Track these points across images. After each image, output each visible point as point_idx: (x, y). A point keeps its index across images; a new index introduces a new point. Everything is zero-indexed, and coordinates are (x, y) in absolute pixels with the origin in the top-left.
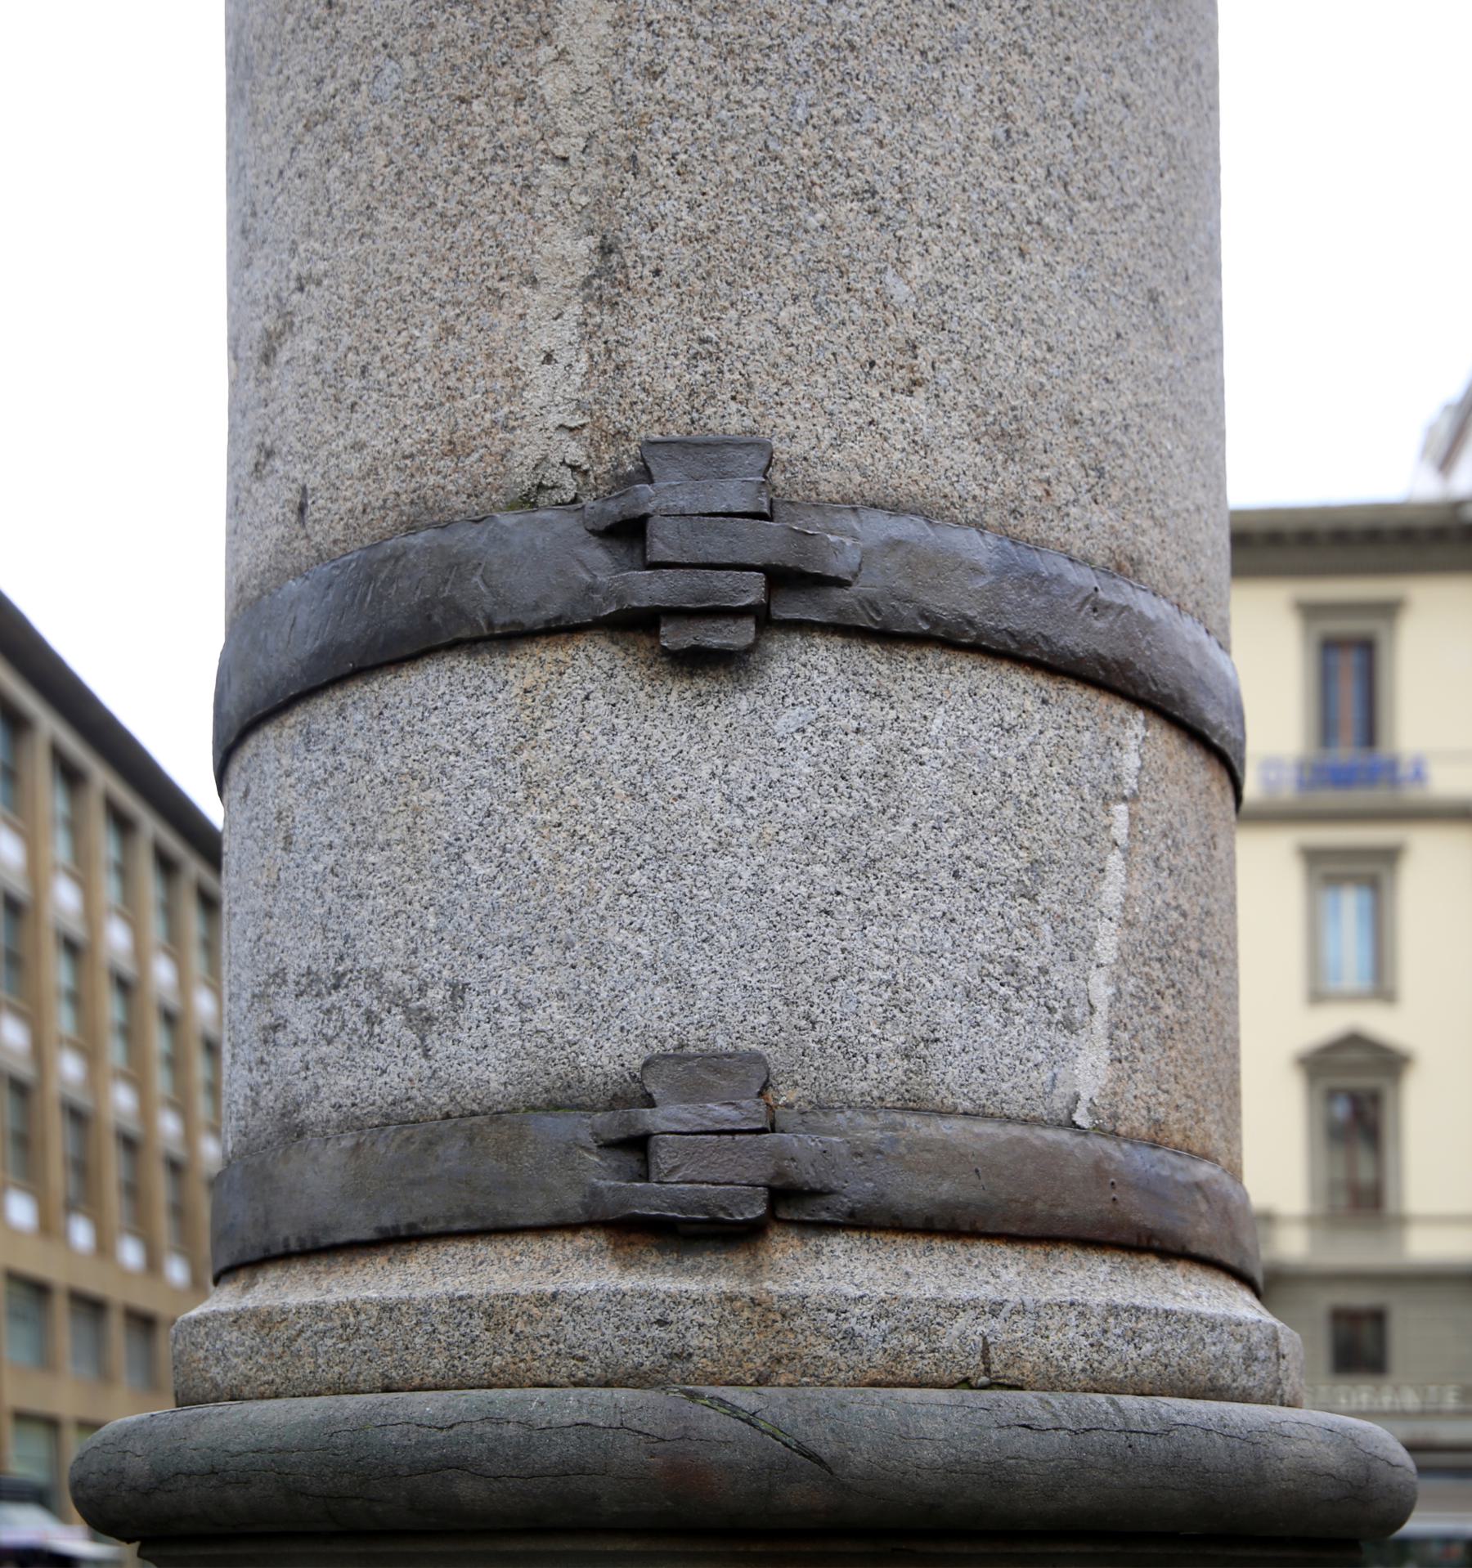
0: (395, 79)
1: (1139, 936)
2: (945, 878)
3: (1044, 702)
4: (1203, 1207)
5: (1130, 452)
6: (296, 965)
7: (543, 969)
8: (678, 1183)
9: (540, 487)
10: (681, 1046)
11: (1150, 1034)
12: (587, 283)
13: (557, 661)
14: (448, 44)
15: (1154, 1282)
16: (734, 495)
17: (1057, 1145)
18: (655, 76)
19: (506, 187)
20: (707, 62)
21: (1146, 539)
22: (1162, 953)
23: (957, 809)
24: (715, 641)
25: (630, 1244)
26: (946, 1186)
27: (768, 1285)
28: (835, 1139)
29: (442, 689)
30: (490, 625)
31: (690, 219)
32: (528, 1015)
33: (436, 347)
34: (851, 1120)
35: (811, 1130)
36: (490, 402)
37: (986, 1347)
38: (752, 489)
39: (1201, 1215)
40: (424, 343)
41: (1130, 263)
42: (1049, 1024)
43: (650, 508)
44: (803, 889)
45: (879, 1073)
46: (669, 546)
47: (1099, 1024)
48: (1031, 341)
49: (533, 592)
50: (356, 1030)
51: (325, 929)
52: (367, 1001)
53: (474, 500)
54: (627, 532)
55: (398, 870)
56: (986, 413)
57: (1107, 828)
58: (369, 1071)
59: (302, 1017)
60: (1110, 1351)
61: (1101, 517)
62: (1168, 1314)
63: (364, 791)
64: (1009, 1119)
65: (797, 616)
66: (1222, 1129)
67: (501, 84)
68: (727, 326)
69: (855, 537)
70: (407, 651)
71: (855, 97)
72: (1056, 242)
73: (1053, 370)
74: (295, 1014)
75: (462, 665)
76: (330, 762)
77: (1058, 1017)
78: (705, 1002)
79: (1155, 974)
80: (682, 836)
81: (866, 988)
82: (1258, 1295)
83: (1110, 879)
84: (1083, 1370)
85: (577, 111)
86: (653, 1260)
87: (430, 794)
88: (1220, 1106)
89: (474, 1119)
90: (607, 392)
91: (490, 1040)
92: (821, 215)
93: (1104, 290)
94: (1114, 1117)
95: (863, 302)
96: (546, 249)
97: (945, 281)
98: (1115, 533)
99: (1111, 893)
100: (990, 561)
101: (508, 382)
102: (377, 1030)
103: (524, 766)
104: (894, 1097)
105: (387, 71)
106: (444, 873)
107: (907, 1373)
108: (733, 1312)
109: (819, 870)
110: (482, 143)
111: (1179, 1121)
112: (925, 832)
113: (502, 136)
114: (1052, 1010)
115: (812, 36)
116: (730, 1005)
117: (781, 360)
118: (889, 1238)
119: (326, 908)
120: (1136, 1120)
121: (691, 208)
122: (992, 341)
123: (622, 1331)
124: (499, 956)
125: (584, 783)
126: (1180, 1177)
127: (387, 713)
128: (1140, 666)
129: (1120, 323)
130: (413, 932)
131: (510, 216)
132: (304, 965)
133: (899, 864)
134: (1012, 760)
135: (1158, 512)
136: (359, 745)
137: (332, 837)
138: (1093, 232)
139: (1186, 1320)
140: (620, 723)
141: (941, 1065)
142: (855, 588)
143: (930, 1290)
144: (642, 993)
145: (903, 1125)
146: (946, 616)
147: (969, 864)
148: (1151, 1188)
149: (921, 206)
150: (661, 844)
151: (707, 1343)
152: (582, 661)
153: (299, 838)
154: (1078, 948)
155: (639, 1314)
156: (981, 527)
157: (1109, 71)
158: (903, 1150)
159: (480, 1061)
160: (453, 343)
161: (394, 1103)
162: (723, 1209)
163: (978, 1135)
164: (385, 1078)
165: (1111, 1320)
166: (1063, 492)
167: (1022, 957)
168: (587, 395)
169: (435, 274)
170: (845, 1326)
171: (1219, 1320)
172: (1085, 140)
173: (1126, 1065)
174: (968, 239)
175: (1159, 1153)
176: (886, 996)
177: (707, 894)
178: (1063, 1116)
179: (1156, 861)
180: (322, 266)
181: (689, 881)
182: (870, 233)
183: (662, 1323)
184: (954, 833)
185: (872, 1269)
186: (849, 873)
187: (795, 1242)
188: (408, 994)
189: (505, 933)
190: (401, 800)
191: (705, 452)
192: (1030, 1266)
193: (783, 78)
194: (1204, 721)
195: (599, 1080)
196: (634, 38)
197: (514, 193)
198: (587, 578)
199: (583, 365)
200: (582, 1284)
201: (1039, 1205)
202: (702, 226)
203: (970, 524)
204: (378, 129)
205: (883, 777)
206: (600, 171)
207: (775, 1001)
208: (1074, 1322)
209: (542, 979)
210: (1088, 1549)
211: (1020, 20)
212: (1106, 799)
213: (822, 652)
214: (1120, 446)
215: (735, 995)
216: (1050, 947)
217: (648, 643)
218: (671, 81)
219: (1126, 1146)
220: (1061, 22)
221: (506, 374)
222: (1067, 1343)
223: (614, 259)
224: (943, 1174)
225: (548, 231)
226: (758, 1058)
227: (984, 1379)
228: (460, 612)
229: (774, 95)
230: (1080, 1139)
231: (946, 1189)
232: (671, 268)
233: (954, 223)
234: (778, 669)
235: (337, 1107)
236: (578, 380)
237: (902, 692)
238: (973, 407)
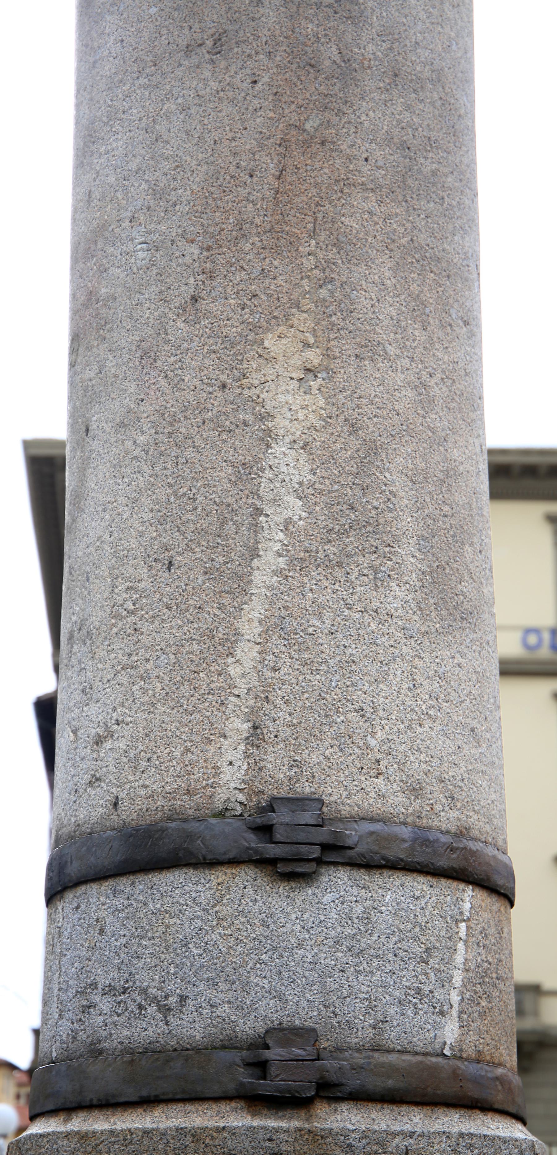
0: (166, 661)
1: (471, 975)
2: (391, 957)
3: (431, 886)
4: (500, 1088)
5: (465, 789)
6: (103, 981)
7: (222, 992)
8: (277, 1082)
9: (226, 809)
10: (280, 1024)
11: (476, 1015)
12: (247, 738)
13: (232, 874)
14: (188, 653)
15: (478, 1122)
16: (308, 818)
17: (437, 1063)
18: (276, 670)
19: (214, 703)
20: (296, 667)
21: (472, 820)
22: (481, 980)
23: (396, 930)
24: (300, 870)
25: (255, 1106)
26: (390, 1082)
27: (315, 1124)
28: (345, 1063)
29: (181, 880)
30: (204, 859)
31: (290, 719)
32: (214, 1009)
33: (182, 755)
34: (351, 1055)
35: (334, 1059)
36: (206, 777)
38: (316, 816)
39: (499, 1091)
40: (177, 753)
41: (463, 721)
43: (275, 821)
44: (333, 962)
45: (363, 1034)
46: (282, 836)
47: (455, 1012)
48: (424, 755)
49: (221, 848)
50: (133, 1012)
51: (119, 969)
52: (139, 1000)
53: (197, 812)
54: (265, 830)
55: (158, 949)
56: (407, 783)
57: (457, 933)
58: (138, 1029)
59: (105, 1004)
61: (453, 814)
62: (485, 1136)
63: (142, 916)
64: (417, 1053)
65: (333, 860)
66: (507, 1051)
67: (212, 669)
68: (304, 756)
69: (356, 831)
70: (166, 865)
71: (355, 678)
72: (433, 719)
73: (433, 764)
74: (101, 1002)
75: (191, 872)
76: (126, 903)
77: (437, 1010)
78: (291, 1006)
79: (478, 990)
80: (283, 941)
81: (358, 1001)
82: (524, 1123)
85: (243, 680)
86: (265, 1112)
87: (174, 920)
88: (506, 1041)
89: (188, 1052)
90: (255, 777)
91: (197, 1019)
92: (342, 718)
93: (453, 732)
94: (461, 1050)
95: (359, 747)
96: (230, 726)
97: (390, 738)
98: (459, 819)
99: (459, 958)
100: (409, 837)
101: (214, 771)
102: (143, 1012)
103: (217, 912)
104: (369, 1045)
105: (162, 658)
106: (179, 951)
108: (301, 1136)
109: (340, 954)
110: (204, 687)
111: (488, 1050)
112: (383, 939)
113: (212, 686)
114: (435, 1008)
115: (338, 658)
116: (301, 1007)
117: (326, 768)
118: (365, 1104)
119: (121, 960)
120: (470, 1052)
121: (290, 715)
122: (409, 757)
123: (253, 1144)
124: (202, 985)
125: (243, 920)
126: (490, 1075)
127: (155, 887)
128: (470, 869)
129: (459, 743)
130: (163, 974)
131: (215, 713)
132: (107, 982)
133: (372, 952)
134: (418, 910)
135: (476, 808)
136: (141, 898)
137: (125, 932)
138: (448, 713)
139: (493, 1139)
140: (259, 898)
141: (388, 1032)
142: (356, 850)
143: (384, 1127)
144: (264, 1002)
145: (373, 1057)
147: (401, 951)
148: (477, 1081)
149: (381, 713)
150: (275, 944)
151: (289, 1149)
152: (243, 874)
153: (108, 930)
154: (445, 982)
155: (260, 1136)
156: (405, 824)
157: (453, 657)
158: (372, 1067)
159: (191, 1027)
160: (189, 755)
161: (150, 1043)
162: (297, 1092)
163: (404, 1060)
164: (146, 1032)
166: (438, 807)
167: (422, 986)
168: (247, 778)
169: (182, 730)
170: (348, 1142)
171: (508, 1139)
172: (444, 682)
173: (466, 1028)
174: (399, 723)
175: (480, 1065)
176: (366, 1004)
177: (293, 964)
178: (439, 1051)
179: (478, 944)
180: (129, 719)
181: (286, 959)
182: (361, 723)
183: (270, 1140)
185: (359, 1117)
186: (352, 956)
187: (326, 1105)
188: (159, 998)
189: (205, 976)
190: (160, 921)
191: (299, 802)
192: (425, 1116)
193: (327, 672)
194: (497, 885)
195: (244, 1037)
196: (267, 658)
197: (217, 705)
198: (247, 844)
199: (245, 767)
200: (236, 1123)
201: (429, 1089)
202: (295, 721)
203: (401, 823)
204: (158, 677)
205: (366, 918)
206: (254, 701)
207: (321, 1006)
208: (444, 1140)
209: (221, 996)
211: (418, 648)
212: (457, 922)
213: (342, 872)
214: (460, 787)
215: (304, 1004)
216: (434, 982)
217: (271, 868)
218: (282, 672)
219: (466, 1063)
220: (434, 645)
221: (213, 768)
223: (259, 731)
224: (389, 1077)
225: (231, 720)
226: (314, 1030)
228: (191, 853)
229: (323, 678)
230: (446, 1061)
231: (390, 1083)
232: (282, 735)
233: (394, 718)
234: (325, 879)
235: (121, 1043)
236: (243, 772)
237: (374, 886)
238: (402, 781)
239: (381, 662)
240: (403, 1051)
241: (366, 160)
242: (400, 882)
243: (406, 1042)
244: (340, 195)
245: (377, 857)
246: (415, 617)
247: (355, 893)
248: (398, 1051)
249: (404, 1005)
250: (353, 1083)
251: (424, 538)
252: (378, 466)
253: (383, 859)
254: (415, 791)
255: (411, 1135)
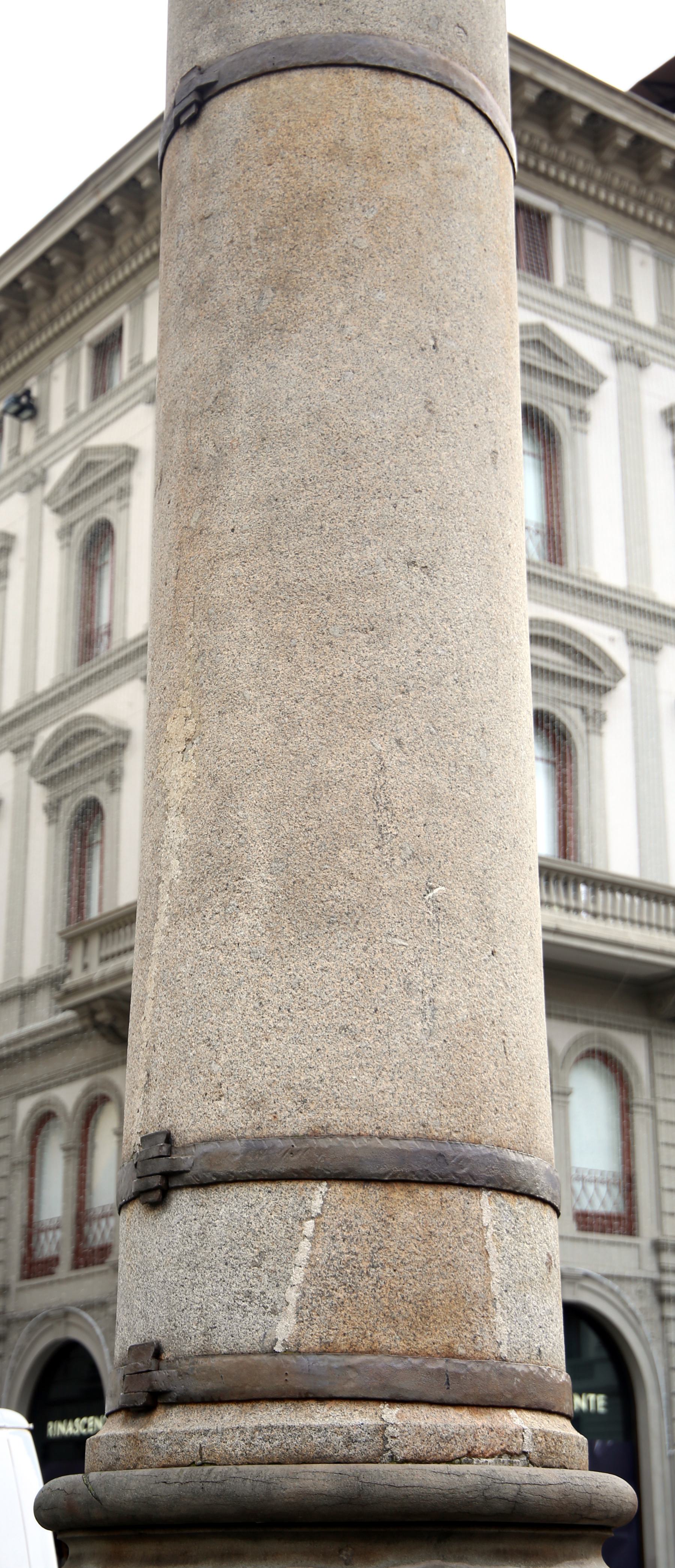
2: (222, 1266)
37: (201, 1448)
42: (264, 1314)
47: (291, 1309)
57: (301, 1232)
60: (255, 1446)
68: (169, 1093)
83: (301, 1250)
84: (242, 1455)
99: (302, 1256)
107: (173, 1461)
112: (216, 1251)
114: (266, 1308)
118: (191, 1406)
146: (222, 1174)
149: (225, 1039)
154: (280, 1280)
165: (257, 1433)
167: (253, 1289)
184: (225, 1249)
205: (202, 1234)
210: (209, 1531)
212: (301, 1221)
222: (235, 1445)
224: (209, 1379)
227: (200, 1462)
231: (209, 1385)
238: (243, 1098)
239: (228, 991)
240: (231, 1354)
241: (233, 530)
242: (234, 1194)
243: (232, 1344)
244: (210, 572)
245: (208, 1176)
246: (264, 938)
247: (194, 1212)
248: (342, 1352)
249: (232, 1310)
250: (196, 1387)
251: (277, 860)
252: (232, 808)
253: (214, 1176)
254: (256, 1104)
255: (206, 1433)
